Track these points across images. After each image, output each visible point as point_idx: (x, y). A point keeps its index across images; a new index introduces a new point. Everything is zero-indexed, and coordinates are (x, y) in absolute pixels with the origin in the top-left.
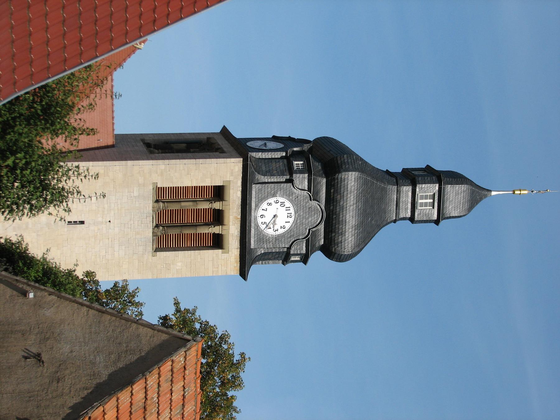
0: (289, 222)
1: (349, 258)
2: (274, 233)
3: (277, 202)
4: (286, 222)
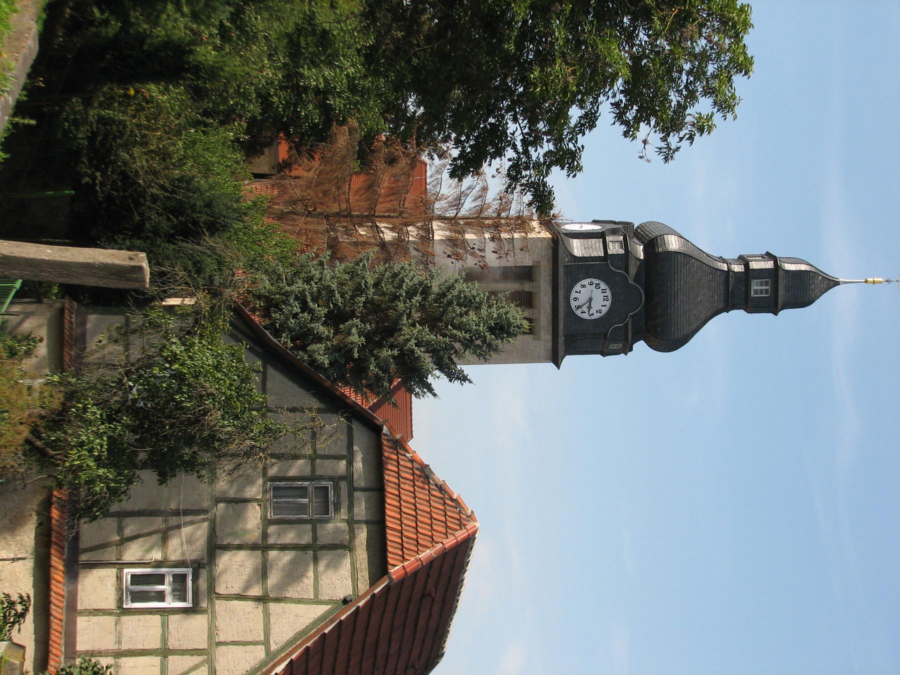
0: (606, 306)
1: (441, 567)
2: (589, 318)
3: (591, 284)
4: (602, 306)
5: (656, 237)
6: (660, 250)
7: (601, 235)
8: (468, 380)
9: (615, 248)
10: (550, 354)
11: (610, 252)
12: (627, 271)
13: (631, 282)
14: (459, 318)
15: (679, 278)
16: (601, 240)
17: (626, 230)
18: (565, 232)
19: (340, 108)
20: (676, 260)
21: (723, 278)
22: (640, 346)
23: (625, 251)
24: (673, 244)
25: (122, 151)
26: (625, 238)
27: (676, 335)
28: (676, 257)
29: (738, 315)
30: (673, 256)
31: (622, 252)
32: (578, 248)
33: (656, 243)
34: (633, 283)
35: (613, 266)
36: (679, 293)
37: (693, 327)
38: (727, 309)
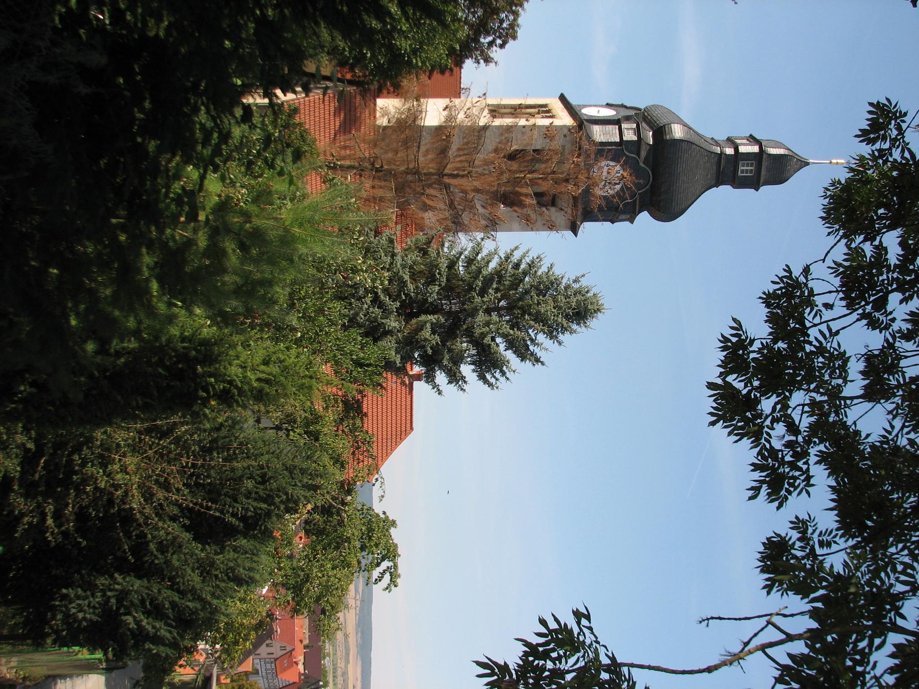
5: (664, 126)
6: (668, 137)
7: (617, 122)
9: (630, 136)
10: (569, 224)
11: (625, 139)
12: (638, 154)
13: (642, 165)
14: (536, 307)
19: (406, 49)
21: (716, 159)
22: (644, 217)
24: (678, 132)
25: (33, 475)
26: (638, 126)
29: (725, 190)
31: (635, 138)
32: (599, 134)
37: (690, 203)
38: (717, 185)
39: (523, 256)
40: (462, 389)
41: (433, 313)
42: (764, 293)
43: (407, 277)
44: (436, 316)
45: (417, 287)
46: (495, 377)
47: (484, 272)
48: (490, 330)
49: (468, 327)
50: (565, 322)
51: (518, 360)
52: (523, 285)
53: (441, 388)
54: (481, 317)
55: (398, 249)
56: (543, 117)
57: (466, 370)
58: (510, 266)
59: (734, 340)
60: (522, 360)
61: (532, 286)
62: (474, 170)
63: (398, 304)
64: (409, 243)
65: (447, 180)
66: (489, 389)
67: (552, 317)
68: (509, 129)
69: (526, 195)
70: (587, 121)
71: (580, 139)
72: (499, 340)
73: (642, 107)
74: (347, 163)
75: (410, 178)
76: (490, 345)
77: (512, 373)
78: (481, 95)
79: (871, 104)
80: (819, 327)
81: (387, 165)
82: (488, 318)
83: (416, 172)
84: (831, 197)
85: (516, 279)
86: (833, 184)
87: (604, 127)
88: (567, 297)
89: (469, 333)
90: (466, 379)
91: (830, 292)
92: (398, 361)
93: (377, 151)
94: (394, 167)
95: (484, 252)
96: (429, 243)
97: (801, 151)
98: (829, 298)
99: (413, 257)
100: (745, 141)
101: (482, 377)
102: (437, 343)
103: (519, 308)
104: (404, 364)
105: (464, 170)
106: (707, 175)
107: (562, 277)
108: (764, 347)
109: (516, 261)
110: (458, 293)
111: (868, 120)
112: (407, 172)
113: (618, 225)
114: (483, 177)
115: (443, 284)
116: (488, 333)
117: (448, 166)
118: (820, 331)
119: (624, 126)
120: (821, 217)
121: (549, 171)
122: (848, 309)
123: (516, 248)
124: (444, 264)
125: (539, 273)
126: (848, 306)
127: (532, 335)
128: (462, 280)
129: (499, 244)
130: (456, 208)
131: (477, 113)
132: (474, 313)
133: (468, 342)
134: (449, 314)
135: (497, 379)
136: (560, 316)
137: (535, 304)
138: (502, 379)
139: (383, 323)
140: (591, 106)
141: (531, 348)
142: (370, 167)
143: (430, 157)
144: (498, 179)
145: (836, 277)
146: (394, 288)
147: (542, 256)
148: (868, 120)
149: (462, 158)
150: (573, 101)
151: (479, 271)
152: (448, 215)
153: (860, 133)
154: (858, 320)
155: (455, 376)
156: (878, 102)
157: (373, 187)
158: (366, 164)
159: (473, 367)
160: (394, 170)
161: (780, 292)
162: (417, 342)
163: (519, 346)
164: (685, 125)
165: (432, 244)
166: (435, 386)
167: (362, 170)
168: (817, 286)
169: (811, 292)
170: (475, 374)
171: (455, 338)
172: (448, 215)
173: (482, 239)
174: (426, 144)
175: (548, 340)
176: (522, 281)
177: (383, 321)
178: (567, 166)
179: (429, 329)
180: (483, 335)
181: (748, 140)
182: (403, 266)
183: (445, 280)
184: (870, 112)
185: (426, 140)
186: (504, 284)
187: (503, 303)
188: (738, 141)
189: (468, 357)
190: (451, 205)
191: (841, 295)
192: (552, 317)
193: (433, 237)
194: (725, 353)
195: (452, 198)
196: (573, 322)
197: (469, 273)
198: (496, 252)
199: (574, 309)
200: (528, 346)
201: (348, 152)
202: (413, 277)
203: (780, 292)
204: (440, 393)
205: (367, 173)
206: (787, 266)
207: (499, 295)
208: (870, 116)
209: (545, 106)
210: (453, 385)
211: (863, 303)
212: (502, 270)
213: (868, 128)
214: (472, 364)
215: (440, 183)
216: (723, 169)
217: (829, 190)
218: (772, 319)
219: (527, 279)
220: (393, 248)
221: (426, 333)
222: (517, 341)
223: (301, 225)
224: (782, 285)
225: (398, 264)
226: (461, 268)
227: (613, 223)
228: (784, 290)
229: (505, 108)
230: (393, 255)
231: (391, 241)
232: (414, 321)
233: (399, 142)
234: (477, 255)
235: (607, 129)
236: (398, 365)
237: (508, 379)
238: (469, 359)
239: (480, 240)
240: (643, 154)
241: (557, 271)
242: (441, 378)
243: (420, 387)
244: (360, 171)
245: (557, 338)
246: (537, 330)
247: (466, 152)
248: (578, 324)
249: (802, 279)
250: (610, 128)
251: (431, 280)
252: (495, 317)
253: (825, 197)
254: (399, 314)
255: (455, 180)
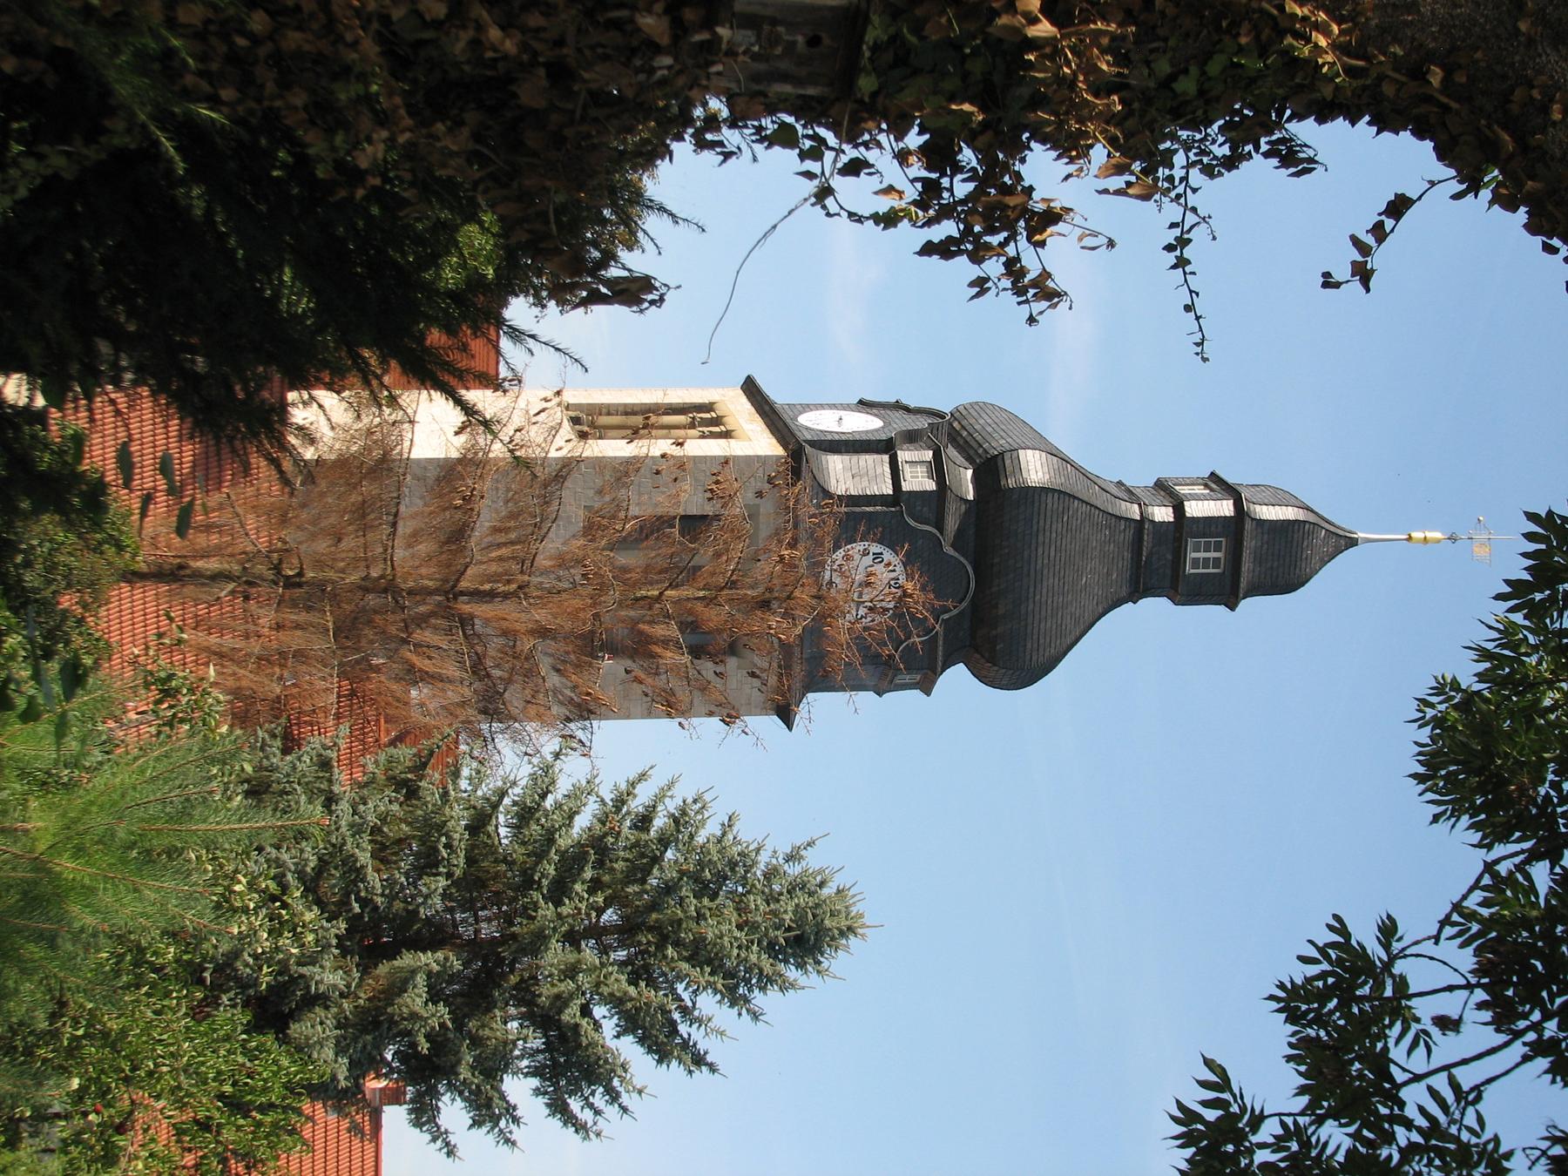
5: (1002, 454)
6: (1011, 483)
7: (885, 447)
8: (707, 1064)
9: (918, 480)
11: (906, 487)
12: (940, 526)
14: (693, 925)
15: (1047, 541)
16: (886, 458)
17: (935, 432)
18: (809, 437)
20: (1043, 506)
21: (1130, 534)
22: (957, 678)
23: (938, 484)
24: (1034, 469)
26: (937, 455)
27: (1034, 658)
28: (1043, 498)
29: (1155, 608)
30: (1037, 497)
31: (931, 485)
33: (1001, 468)
34: (951, 552)
35: (909, 515)
36: (1045, 572)
38: (1134, 596)
39: (660, 797)
40: (507, 1141)
41: (432, 945)
42: (1281, 986)
43: (364, 858)
44: (440, 955)
45: (391, 882)
46: (591, 1106)
47: (563, 842)
48: (579, 988)
49: (522, 980)
50: (766, 963)
51: (650, 1060)
52: (661, 869)
53: (452, 1139)
54: (555, 954)
55: (342, 781)
56: (703, 436)
57: (519, 1089)
58: (628, 823)
59: (1211, 1115)
60: (660, 1061)
61: (682, 873)
62: (535, 580)
63: (343, 926)
64: (371, 768)
65: (465, 606)
66: (577, 1138)
67: (735, 952)
68: (625, 470)
69: (665, 642)
70: (813, 444)
71: (797, 502)
72: (599, 1011)
73: (946, 408)
74: (213, 565)
75: (372, 600)
76: (577, 1026)
77: (635, 1095)
78: (549, 394)
79: (1532, 517)
80: (1431, 1081)
81: (313, 569)
82: (572, 957)
83: (388, 587)
84: (1438, 722)
85: (643, 855)
86: (1439, 689)
87: (855, 458)
88: (771, 898)
89: (525, 994)
90: (519, 1113)
91: (1450, 988)
92: (342, 1073)
93: (290, 535)
94: (331, 574)
95: (563, 786)
96: (420, 767)
97: (1340, 516)
98: (1450, 1005)
99: (382, 803)
100: (1199, 490)
101: (559, 1108)
102: (442, 1025)
103: (651, 929)
104: (356, 1079)
105: (509, 582)
106: (1108, 574)
107: (758, 850)
108: (1287, 1134)
109: (641, 809)
110: (497, 893)
111: (1525, 555)
112: (366, 587)
113: (891, 697)
114: (556, 598)
115: (458, 872)
116: (571, 996)
117: (469, 572)
118: (1430, 1089)
119: (903, 455)
120: (1415, 776)
121: (721, 581)
122: (1498, 1030)
123: (642, 777)
124: (458, 819)
125: (700, 839)
126: (1499, 1023)
127: (686, 996)
128: (505, 861)
129: (597, 762)
130: (488, 675)
131: (540, 440)
132: (538, 942)
133: (522, 1017)
134: (474, 948)
135: (597, 1112)
136: (755, 948)
137: (691, 918)
138: (611, 1111)
139: (302, 976)
140: (821, 406)
141: (683, 1029)
142: (270, 575)
143: (423, 548)
144: (594, 605)
145: (1462, 946)
146: (332, 884)
147: (707, 797)
148: (1525, 555)
149: (504, 551)
150: (778, 394)
151: (550, 838)
152: (467, 692)
153: (1508, 589)
154: (1526, 1059)
155: (488, 1104)
156: (1550, 513)
157: (279, 627)
158: (261, 569)
159: (534, 1082)
160: (333, 582)
161: (1320, 984)
162: (392, 1022)
163: (653, 1026)
164: (1053, 452)
165: (429, 771)
166: (438, 1135)
167: (248, 583)
168: (1417, 974)
169: (1401, 984)
170: (541, 1100)
171: (488, 1010)
172: (467, 692)
173: (557, 755)
174: (412, 517)
175: (725, 1007)
176: (656, 860)
177: (304, 970)
178: (766, 568)
179: (422, 989)
180: (561, 1001)
181: (1206, 486)
182: (357, 829)
183: (462, 861)
184: (1530, 537)
185: (413, 505)
186: (613, 869)
187: (610, 916)
188: (1183, 490)
189: (521, 1057)
190: (478, 669)
191: (1480, 995)
192: (735, 952)
193: (432, 753)
194: (1190, 1151)
195: (479, 649)
196: (786, 961)
197: (524, 843)
198: (589, 788)
199: (789, 929)
200: (673, 1024)
201: (215, 539)
202: (384, 853)
203: (1320, 984)
204: (451, 1152)
205: (263, 589)
206: (1337, 917)
207: (600, 899)
208: (1532, 547)
209: (708, 407)
210: (485, 1129)
211: (1536, 1016)
212: (605, 835)
213: (1526, 576)
214: (534, 1074)
215: (446, 611)
216: (1150, 555)
217: (1432, 706)
218: (1305, 1053)
219: (669, 854)
220: (330, 781)
221: (415, 999)
222: (647, 1013)
223: (79, 852)
224: (1325, 966)
225: (343, 823)
226: (503, 831)
227: (880, 694)
228: (1331, 980)
229: (609, 414)
230: (330, 801)
231: (325, 764)
232: (383, 969)
233: (345, 512)
234: (543, 796)
235: (862, 463)
236: (343, 1084)
237: (624, 1109)
238: (525, 1063)
239: (549, 758)
240: (952, 523)
241: (746, 833)
242: (453, 1112)
243: (395, 1118)
244: (247, 584)
245: (747, 1001)
246: (698, 983)
247: (513, 536)
248: (801, 966)
249: (1376, 951)
250: (868, 460)
251: (428, 862)
252: (589, 953)
253: (1422, 722)
254: (345, 952)
255: (485, 607)
